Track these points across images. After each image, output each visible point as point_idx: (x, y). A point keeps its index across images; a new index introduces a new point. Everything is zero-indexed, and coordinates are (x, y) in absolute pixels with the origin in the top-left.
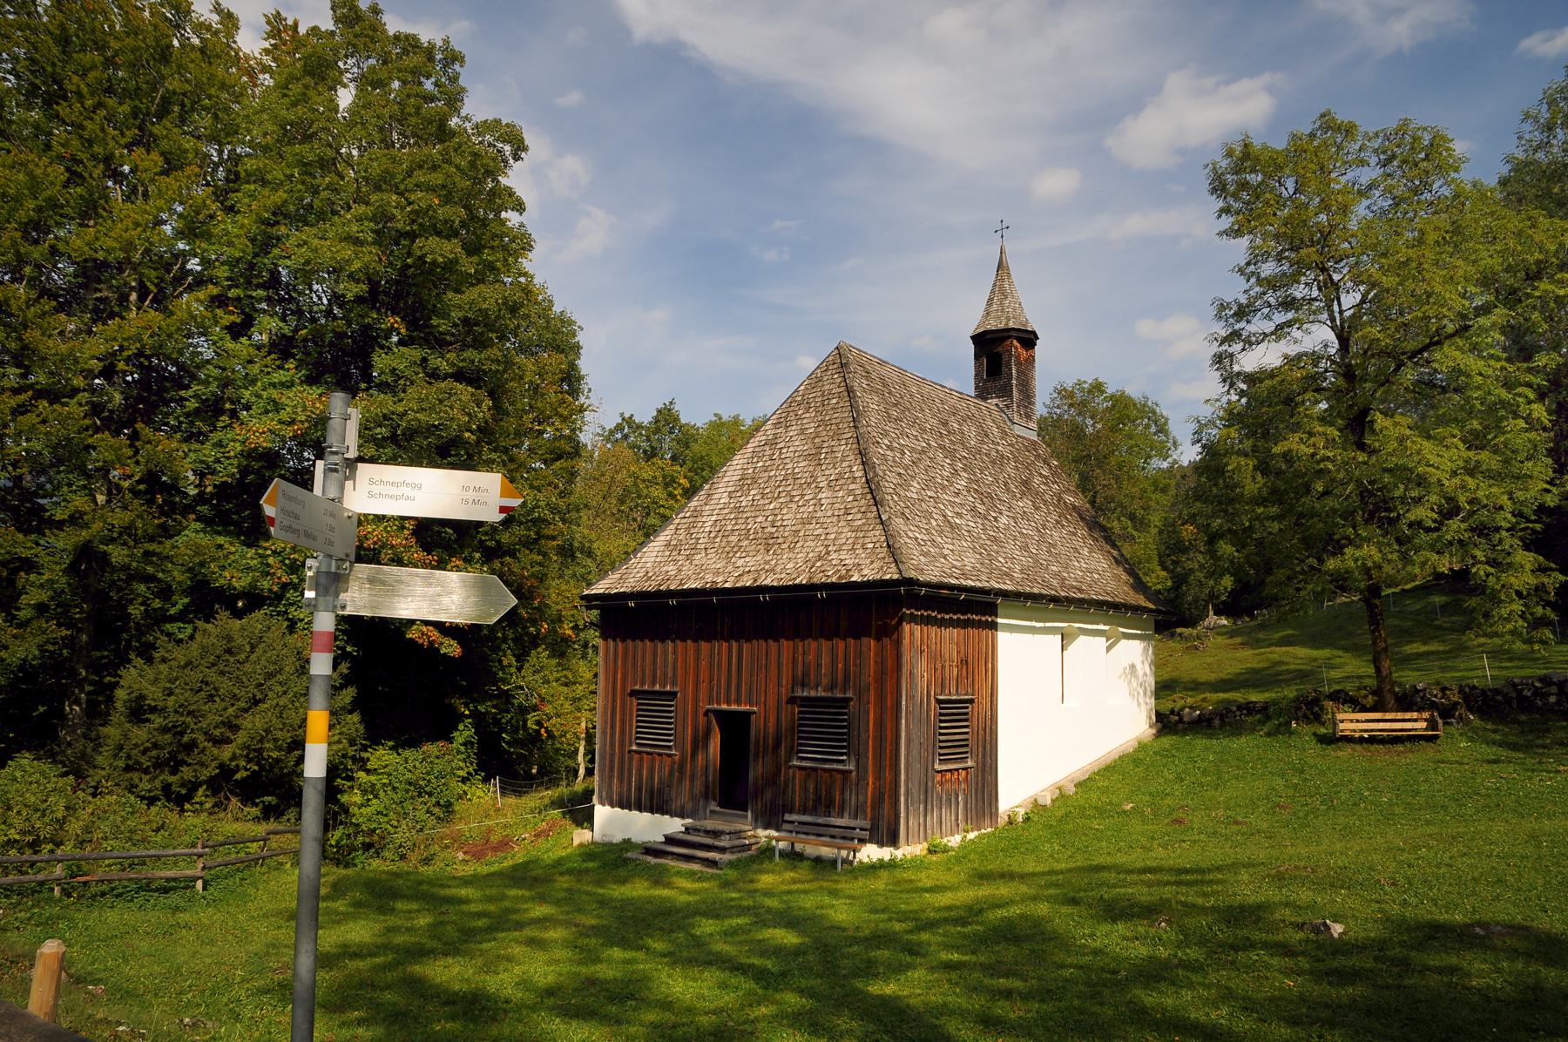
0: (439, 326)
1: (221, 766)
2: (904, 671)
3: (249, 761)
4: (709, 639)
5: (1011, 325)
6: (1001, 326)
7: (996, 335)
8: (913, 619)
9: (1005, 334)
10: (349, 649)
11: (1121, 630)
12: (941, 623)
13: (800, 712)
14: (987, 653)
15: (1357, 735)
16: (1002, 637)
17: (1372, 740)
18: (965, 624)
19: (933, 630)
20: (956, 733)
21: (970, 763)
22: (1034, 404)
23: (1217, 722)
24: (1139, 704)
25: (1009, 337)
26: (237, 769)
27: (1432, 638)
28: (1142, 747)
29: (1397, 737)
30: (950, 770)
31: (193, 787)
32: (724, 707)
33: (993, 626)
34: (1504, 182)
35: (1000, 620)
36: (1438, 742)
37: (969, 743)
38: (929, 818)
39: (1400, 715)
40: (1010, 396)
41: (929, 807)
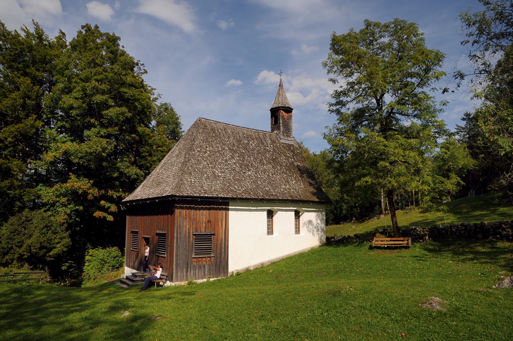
0: (103, 121)
1: (20, 254)
2: (176, 225)
3: (28, 252)
4: (136, 215)
5: (280, 105)
6: (277, 106)
7: (275, 109)
8: (176, 208)
9: (278, 109)
10: (77, 219)
11: (304, 209)
12: (200, 209)
13: (158, 238)
14: (222, 218)
15: (383, 246)
16: (231, 213)
17: (389, 248)
18: (210, 209)
19: (193, 211)
20: (205, 245)
21: (212, 255)
22: (291, 132)
23: (345, 241)
24: (313, 234)
25: (280, 110)
26: (24, 255)
27: (485, 209)
28: (312, 252)
29: (397, 247)
30: (205, 257)
31: (13, 260)
32: (146, 236)
33: (228, 210)
34: (361, 32)
35: (230, 207)
36: (409, 249)
37: (194, 249)
38: (189, 273)
39: (396, 239)
40: (280, 130)
41: (189, 269)
